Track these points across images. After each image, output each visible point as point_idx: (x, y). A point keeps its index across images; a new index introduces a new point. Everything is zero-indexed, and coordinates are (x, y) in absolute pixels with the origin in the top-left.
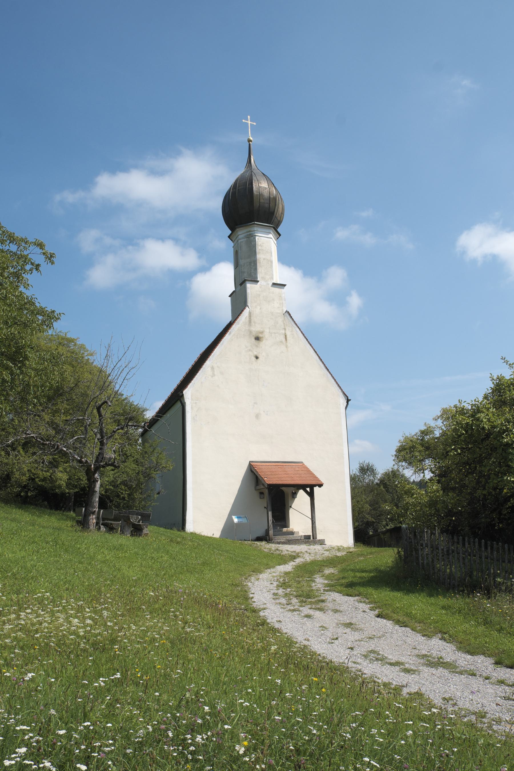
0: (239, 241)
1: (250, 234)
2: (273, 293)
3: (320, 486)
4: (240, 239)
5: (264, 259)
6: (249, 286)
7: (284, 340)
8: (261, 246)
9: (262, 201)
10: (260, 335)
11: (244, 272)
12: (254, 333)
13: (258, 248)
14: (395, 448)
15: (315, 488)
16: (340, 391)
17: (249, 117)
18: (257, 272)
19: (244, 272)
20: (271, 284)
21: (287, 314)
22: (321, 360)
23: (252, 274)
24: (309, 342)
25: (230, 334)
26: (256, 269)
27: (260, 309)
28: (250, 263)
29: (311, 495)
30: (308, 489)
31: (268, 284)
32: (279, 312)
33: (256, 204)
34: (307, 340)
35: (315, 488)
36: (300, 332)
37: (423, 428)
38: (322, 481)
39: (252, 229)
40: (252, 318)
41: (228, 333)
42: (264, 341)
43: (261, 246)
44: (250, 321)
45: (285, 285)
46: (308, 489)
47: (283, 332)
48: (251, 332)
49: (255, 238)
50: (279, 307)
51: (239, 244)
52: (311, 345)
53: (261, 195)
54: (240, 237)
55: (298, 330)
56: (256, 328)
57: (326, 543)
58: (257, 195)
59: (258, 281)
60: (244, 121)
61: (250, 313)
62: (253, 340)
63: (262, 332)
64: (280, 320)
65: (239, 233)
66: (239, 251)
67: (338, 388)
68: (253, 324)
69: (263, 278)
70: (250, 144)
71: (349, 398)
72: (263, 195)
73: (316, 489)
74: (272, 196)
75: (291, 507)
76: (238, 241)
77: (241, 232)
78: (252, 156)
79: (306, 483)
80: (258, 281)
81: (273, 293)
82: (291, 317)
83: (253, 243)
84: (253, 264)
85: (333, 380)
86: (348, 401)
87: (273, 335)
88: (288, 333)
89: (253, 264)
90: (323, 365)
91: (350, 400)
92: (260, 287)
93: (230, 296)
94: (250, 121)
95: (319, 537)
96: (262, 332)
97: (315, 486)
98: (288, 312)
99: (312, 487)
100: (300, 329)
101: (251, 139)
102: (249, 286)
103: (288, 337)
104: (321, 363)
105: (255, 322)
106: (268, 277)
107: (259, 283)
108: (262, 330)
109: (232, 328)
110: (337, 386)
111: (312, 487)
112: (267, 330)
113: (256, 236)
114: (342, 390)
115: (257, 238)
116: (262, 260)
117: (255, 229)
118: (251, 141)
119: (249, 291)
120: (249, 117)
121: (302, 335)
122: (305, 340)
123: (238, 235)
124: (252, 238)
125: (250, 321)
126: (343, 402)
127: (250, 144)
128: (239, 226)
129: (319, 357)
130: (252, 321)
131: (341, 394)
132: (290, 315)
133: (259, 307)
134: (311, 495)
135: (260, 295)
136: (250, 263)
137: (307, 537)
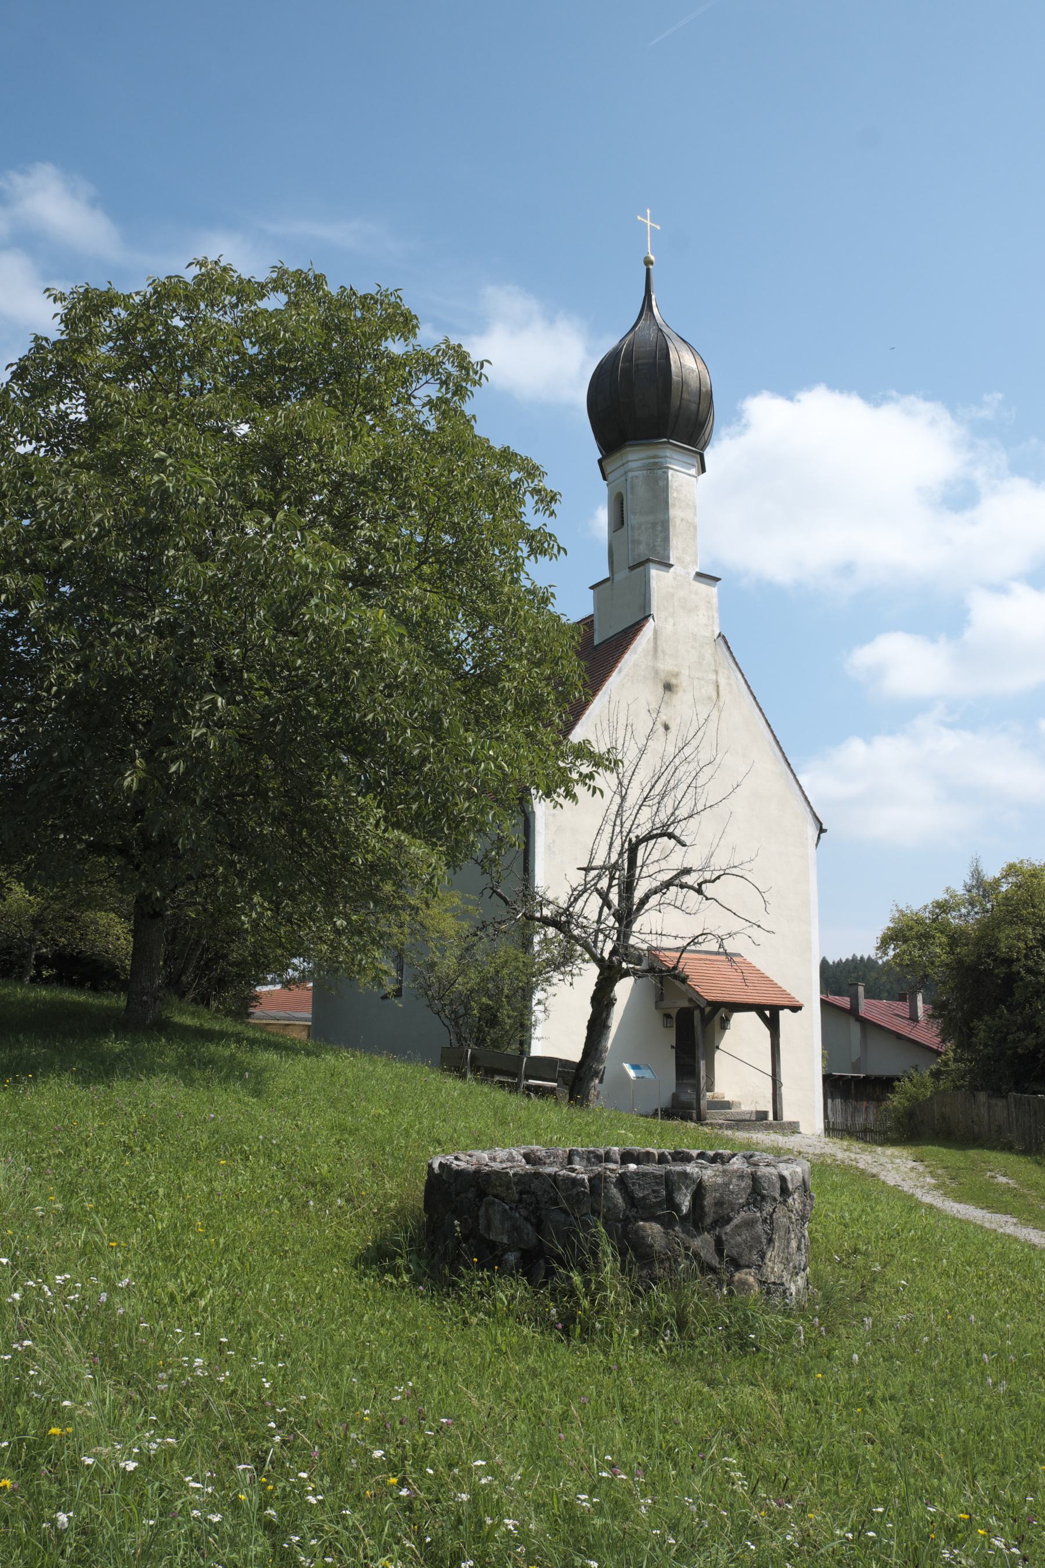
0: (630, 474)
1: (655, 464)
2: (697, 594)
3: (796, 1008)
4: (631, 470)
5: (682, 520)
6: (655, 573)
7: (714, 695)
8: (678, 492)
9: (685, 396)
10: (674, 681)
11: (639, 542)
12: (662, 675)
13: (673, 495)
14: (880, 934)
15: (781, 1012)
16: (808, 810)
17: (648, 211)
18: (668, 546)
19: (639, 542)
20: (693, 574)
21: (720, 641)
22: (778, 743)
23: (658, 548)
24: (757, 704)
25: (620, 671)
26: (666, 539)
27: (674, 624)
28: (654, 525)
29: (773, 1024)
30: (767, 1013)
31: (688, 573)
32: (707, 635)
33: (675, 402)
34: (755, 698)
35: (781, 1012)
36: (742, 681)
37: (941, 896)
38: (797, 998)
39: (661, 453)
40: (659, 643)
41: (617, 670)
42: (680, 694)
43: (678, 492)
44: (655, 649)
45: (717, 579)
46: (767, 1013)
47: (714, 677)
48: (656, 672)
49: (666, 473)
50: (706, 625)
51: (629, 480)
52: (760, 710)
53: (683, 383)
54: (632, 465)
55: (740, 676)
56: (666, 665)
57: (801, 1129)
58: (678, 382)
59: (672, 566)
60: (639, 218)
61: (656, 632)
62: (661, 689)
63: (676, 675)
64: (708, 651)
65: (631, 457)
66: (629, 496)
67: (805, 804)
68: (660, 655)
69: (678, 559)
70: (648, 271)
71: (824, 827)
72: (689, 386)
73: (784, 1015)
74: (703, 389)
75: (718, 1048)
76: (626, 473)
77: (635, 458)
78: (653, 297)
79: (720, 999)
80: (672, 566)
81: (697, 594)
82: (729, 648)
83: (661, 483)
84: (659, 528)
85: (797, 788)
86: (822, 830)
87: (696, 682)
88: (722, 682)
89: (659, 528)
90: (779, 754)
91: (825, 831)
92: (675, 579)
93: (591, 588)
94: (651, 221)
95: (788, 1116)
96: (676, 675)
97: (783, 1007)
98: (724, 637)
99: (775, 1009)
100: (743, 675)
101: (652, 258)
102: (655, 573)
103: (721, 688)
104: (777, 750)
105: (663, 652)
106: (688, 559)
107: (672, 569)
108: (676, 669)
109: (623, 661)
110: (803, 799)
111: (775, 1009)
112: (685, 672)
113: (668, 468)
114: (811, 808)
115: (670, 472)
116: (678, 522)
117: (668, 454)
118: (652, 263)
119: (654, 584)
120: (648, 211)
121: (746, 687)
122: (752, 699)
123: (628, 462)
124: (660, 472)
125: (655, 649)
126: (812, 831)
127: (648, 271)
128: (632, 442)
129: (775, 737)
130: (659, 649)
131: (810, 817)
132: (726, 643)
133: (671, 621)
134: (773, 1024)
135: (673, 595)
136: (654, 525)
137: (762, 1116)
